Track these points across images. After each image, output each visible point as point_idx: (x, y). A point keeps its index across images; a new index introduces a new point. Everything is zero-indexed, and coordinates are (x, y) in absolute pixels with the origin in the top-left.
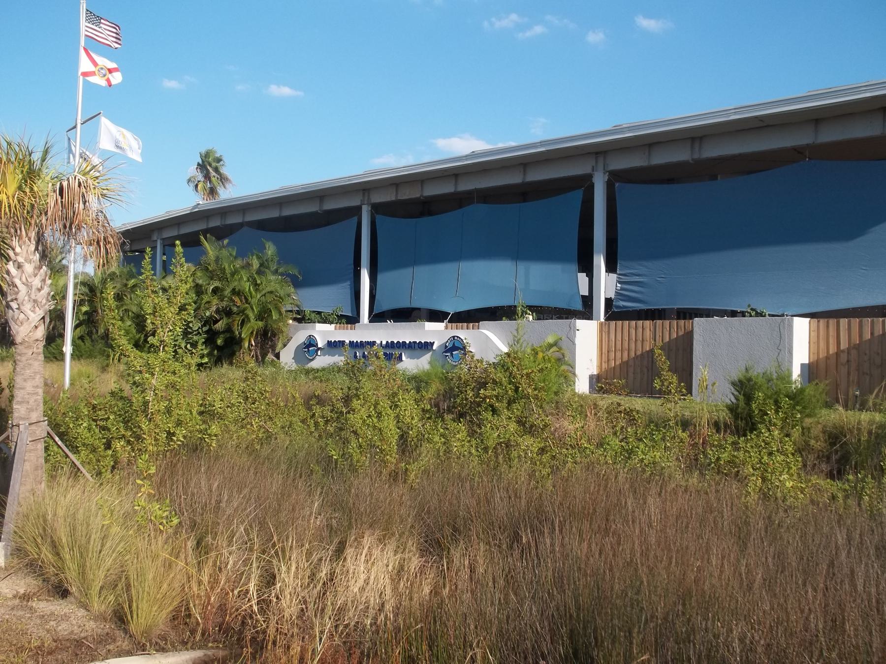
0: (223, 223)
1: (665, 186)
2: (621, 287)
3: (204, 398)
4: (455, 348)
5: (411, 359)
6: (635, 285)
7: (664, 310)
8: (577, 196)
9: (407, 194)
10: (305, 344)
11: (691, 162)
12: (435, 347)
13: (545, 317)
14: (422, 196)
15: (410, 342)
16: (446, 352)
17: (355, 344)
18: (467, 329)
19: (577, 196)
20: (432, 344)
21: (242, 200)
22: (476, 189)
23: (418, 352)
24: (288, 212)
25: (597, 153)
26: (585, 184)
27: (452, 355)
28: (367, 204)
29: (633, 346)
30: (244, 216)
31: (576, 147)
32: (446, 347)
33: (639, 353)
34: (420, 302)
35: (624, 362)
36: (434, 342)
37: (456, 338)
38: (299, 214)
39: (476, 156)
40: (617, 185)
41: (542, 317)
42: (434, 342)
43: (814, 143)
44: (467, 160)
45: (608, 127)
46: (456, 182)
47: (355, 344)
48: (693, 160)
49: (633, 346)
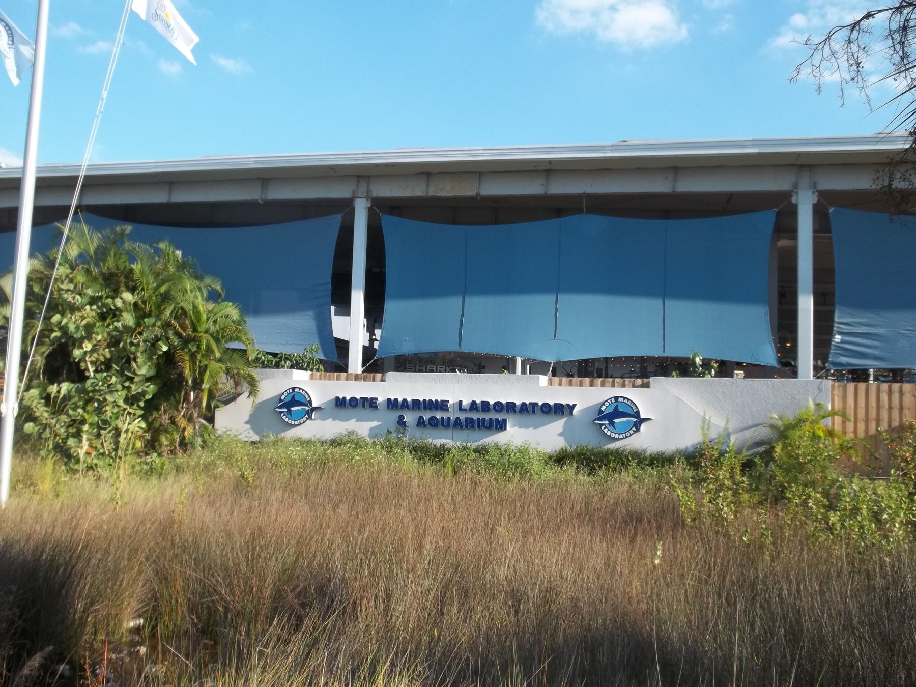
0: (263, 197)
1: (661, 223)
2: (841, 340)
3: (639, 520)
4: (293, 402)
5: (520, 427)
6: (867, 338)
7: (902, 370)
8: (336, 220)
9: (446, 190)
10: (281, 401)
11: (260, 201)
12: (575, 411)
13: (438, 369)
14: (478, 195)
15: (425, 401)
16: (600, 419)
17: (399, 404)
18: (559, 385)
19: (336, 220)
20: (571, 408)
21: (64, 171)
22: (584, 193)
23: (538, 418)
24: (182, 196)
25: (359, 177)
26: (346, 207)
27: (289, 411)
28: (367, 198)
29: (884, 415)
30: (170, 193)
31: (799, 154)
32: (601, 412)
33: (895, 424)
34: (473, 345)
35: (872, 436)
36: (574, 405)
37: (297, 390)
38: (241, 201)
39: (628, 147)
40: (831, 210)
41: (435, 369)
42: (574, 405)
43: (545, 193)
44: (612, 151)
45: (869, 132)
46: (480, 181)
47: (399, 404)
48: (262, 200)
49: (884, 415)
